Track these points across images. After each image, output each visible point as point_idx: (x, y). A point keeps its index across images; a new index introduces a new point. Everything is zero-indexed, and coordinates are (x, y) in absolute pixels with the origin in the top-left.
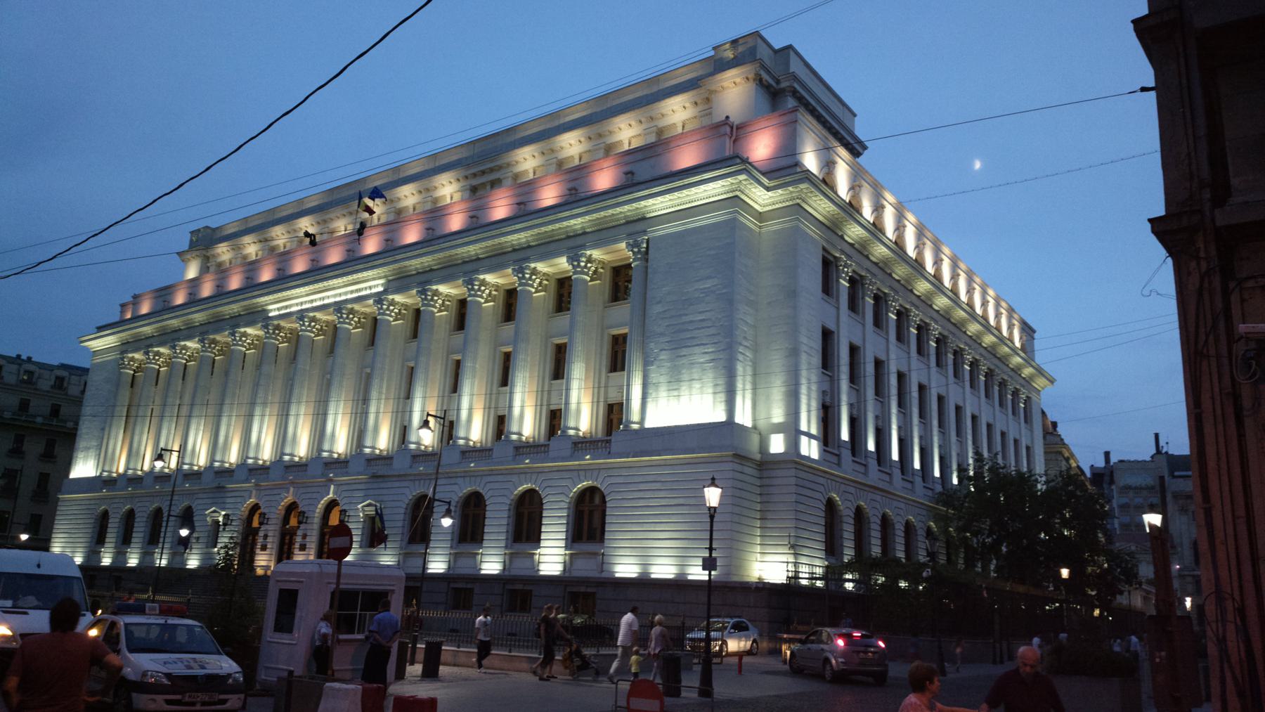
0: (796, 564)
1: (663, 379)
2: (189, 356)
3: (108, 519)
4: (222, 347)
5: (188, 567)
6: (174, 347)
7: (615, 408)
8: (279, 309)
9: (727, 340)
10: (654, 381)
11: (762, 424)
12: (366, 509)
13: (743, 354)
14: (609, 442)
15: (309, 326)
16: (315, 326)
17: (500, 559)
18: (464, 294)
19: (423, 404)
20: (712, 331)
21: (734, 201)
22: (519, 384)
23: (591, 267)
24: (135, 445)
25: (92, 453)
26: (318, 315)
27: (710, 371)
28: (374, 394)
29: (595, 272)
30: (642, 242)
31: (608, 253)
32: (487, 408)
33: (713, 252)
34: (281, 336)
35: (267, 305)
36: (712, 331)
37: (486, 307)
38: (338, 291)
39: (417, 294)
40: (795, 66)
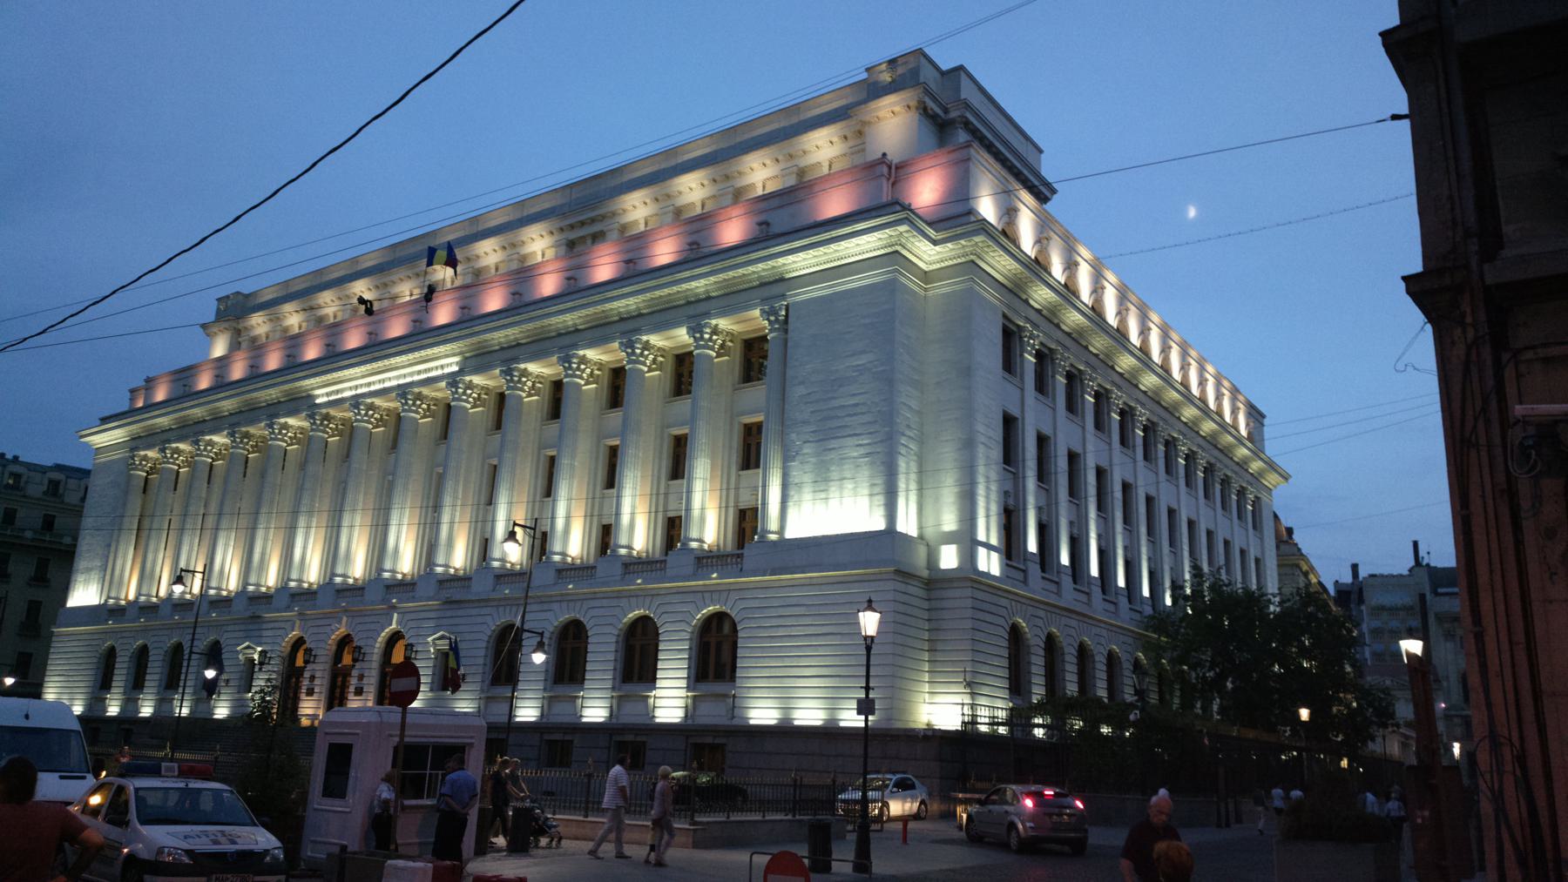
0: (973, 706)
1: (807, 478)
2: (216, 453)
3: (115, 657)
4: (256, 442)
5: (215, 717)
6: (196, 443)
7: (748, 513)
8: (328, 394)
9: (887, 429)
10: (796, 481)
11: (930, 532)
12: (438, 642)
13: (906, 446)
14: (740, 556)
15: (366, 415)
16: (373, 414)
17: (606, 703)
18: (559, 374)
19: (508, 511)
20: (867, 418)
21: (894, 258)
22: (628, 486)
23: (717, 340)
24: (149, 565)
25: (95, 576)
26: (378, 401)
27: (865, 468)
28: (447, 500)
29: (722, 346)
30: (780, 309)
31: (738, 323)
32: (589, 516)
33: (867, 321)
34: (331, 428)
35: (313, 389)
36: (867, 418)
37: (422, 423)
38: (402, 371)
39: (501, 375)
40: (967, 92)
